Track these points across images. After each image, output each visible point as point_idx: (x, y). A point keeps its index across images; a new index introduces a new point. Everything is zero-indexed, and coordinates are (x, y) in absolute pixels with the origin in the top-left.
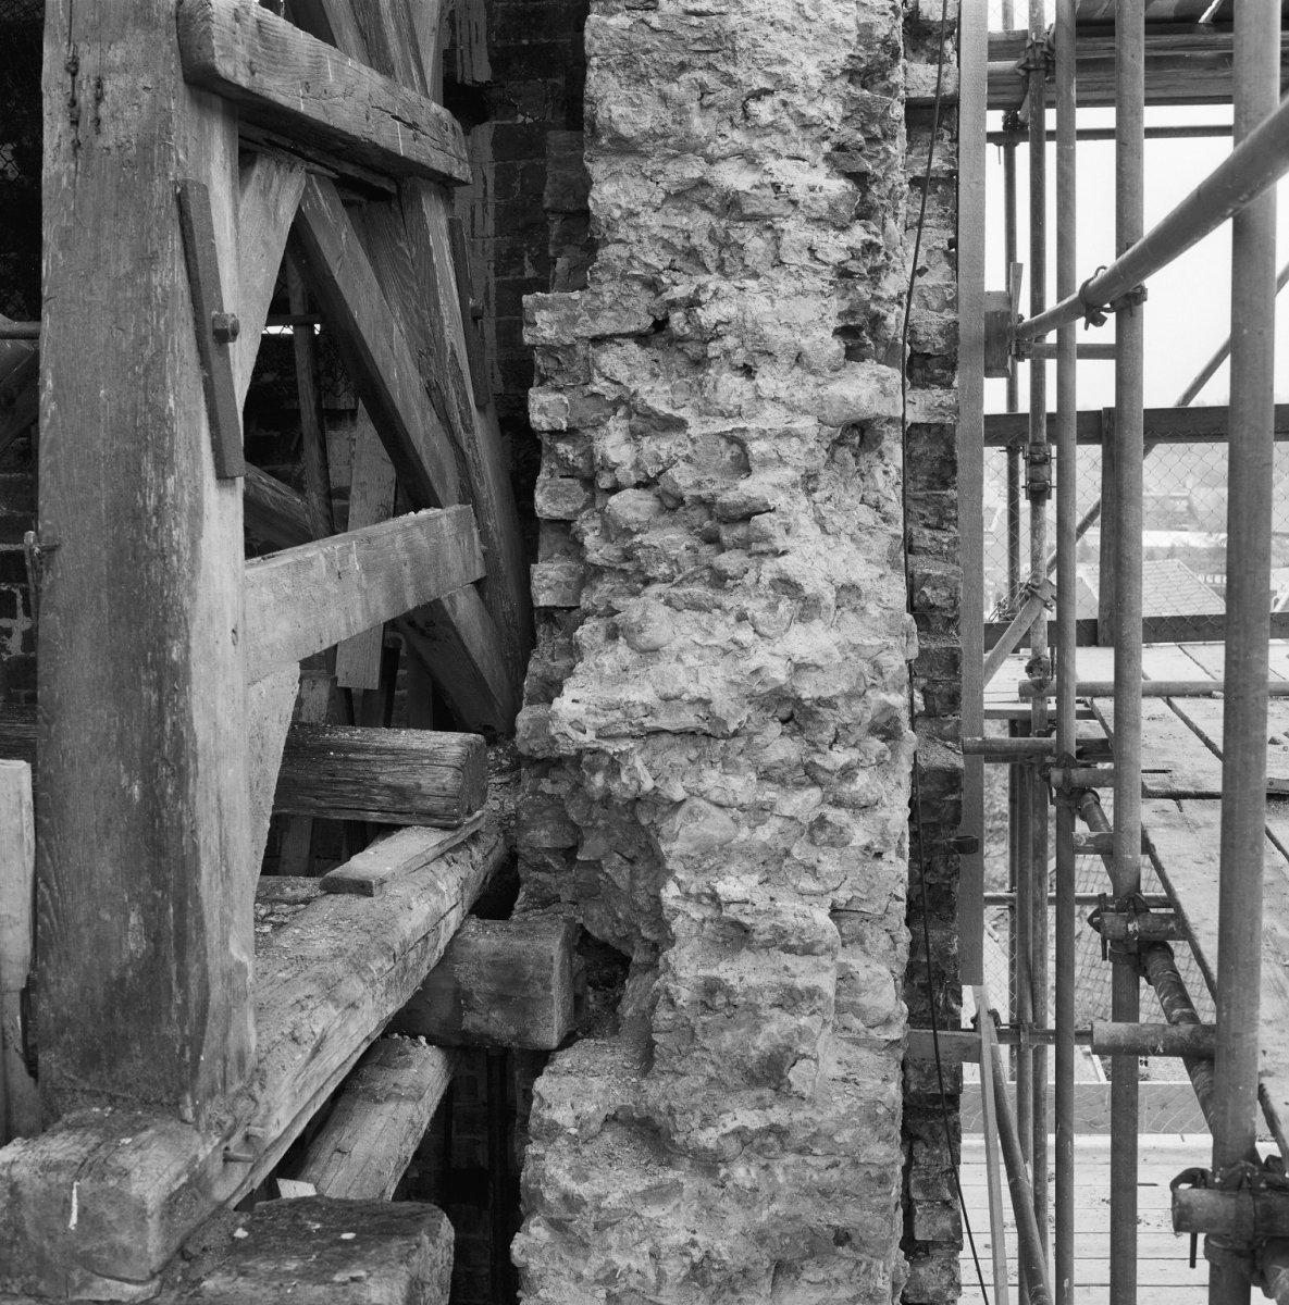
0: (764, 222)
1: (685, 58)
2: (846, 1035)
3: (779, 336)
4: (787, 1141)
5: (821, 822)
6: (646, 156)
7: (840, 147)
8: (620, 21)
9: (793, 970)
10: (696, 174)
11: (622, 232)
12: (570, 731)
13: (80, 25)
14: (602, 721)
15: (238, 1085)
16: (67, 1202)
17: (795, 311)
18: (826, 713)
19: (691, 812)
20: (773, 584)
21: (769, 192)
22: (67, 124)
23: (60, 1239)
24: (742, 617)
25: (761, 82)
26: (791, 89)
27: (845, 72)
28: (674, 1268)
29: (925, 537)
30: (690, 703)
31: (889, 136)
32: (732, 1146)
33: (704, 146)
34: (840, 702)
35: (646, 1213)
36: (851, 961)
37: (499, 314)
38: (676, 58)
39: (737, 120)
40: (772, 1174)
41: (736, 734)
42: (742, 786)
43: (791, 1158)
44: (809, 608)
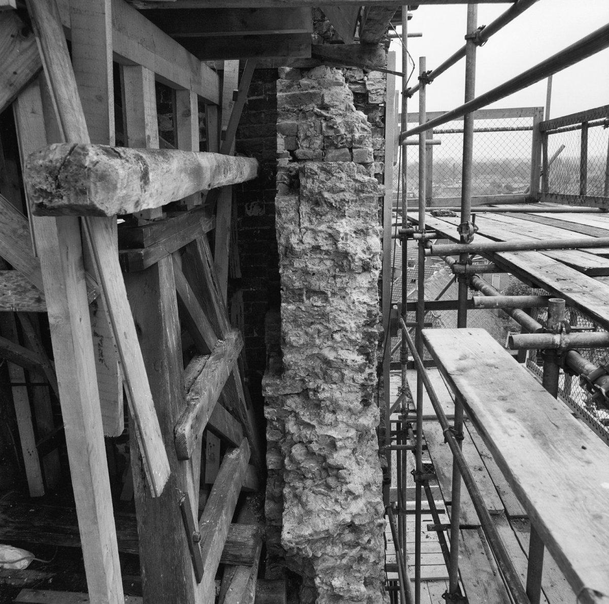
0: (338, 370)
1: (313, 321)
3: (344, 404)
8: (291, 307)
11: (293, 368)
12: (288, 543)
14: (297, 540)
21: (340, 361)
22: (141, 479)
24: (336, 501)
38: (310, 320)
42: (337, 550)
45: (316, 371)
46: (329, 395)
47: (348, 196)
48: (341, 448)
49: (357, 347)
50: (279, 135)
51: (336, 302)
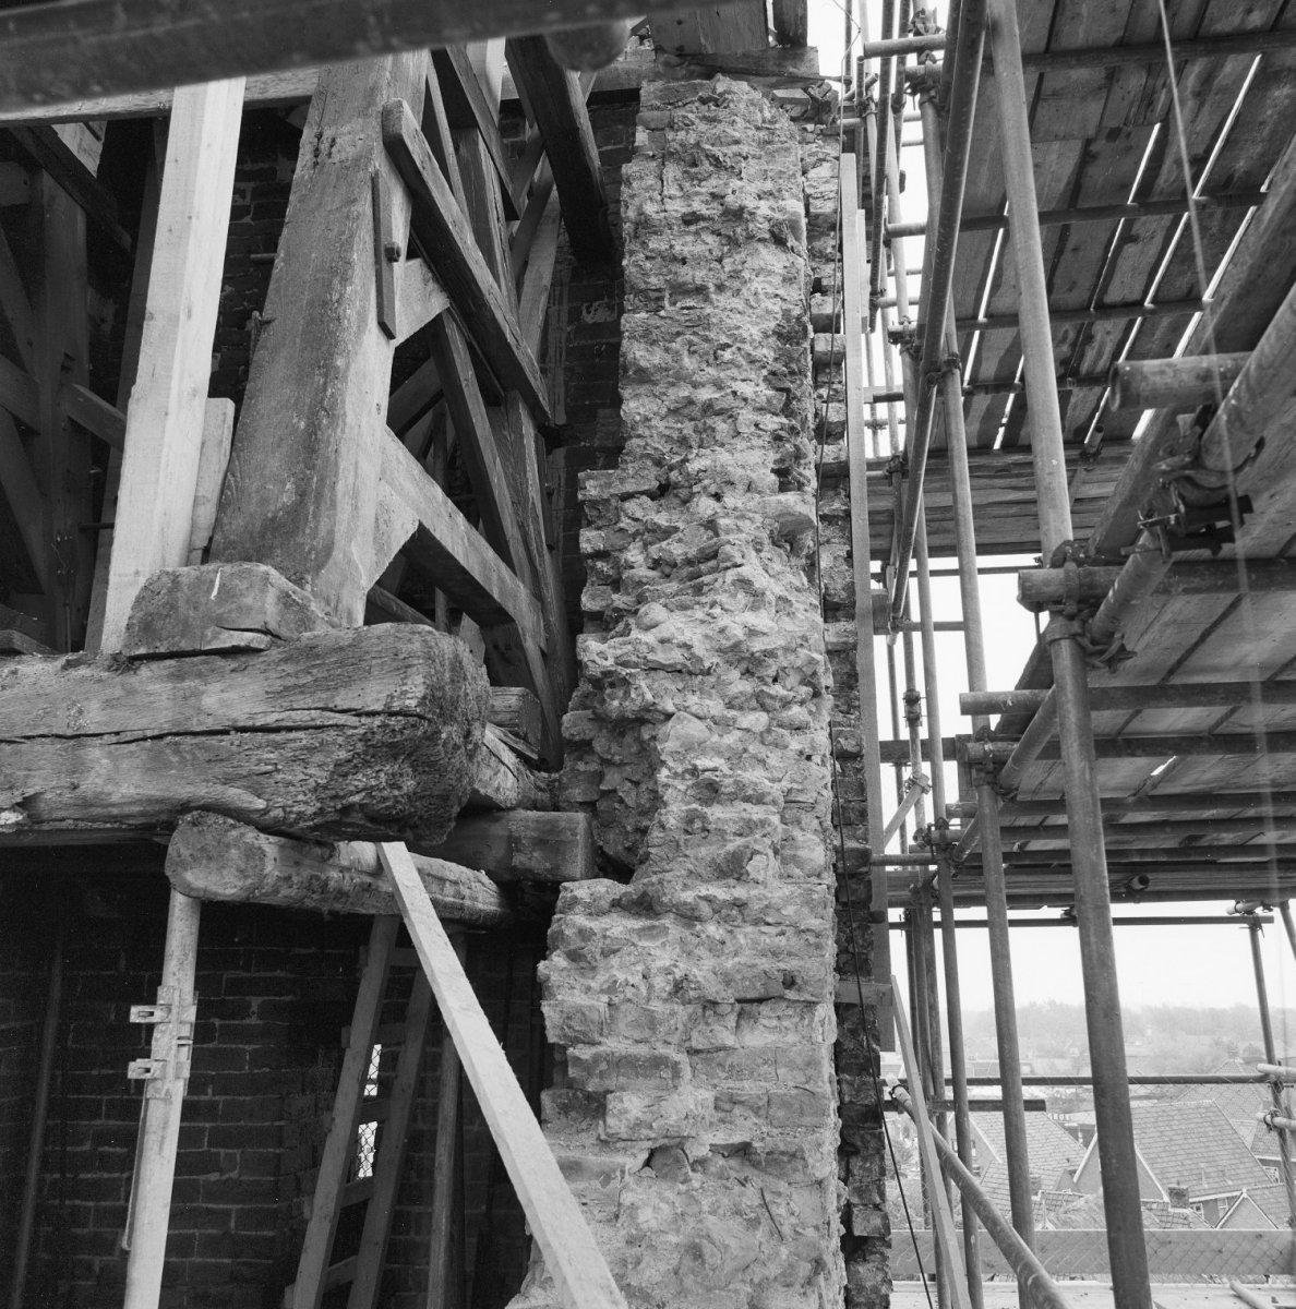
0: (728, 414)
2: (789, 880)
3: (736, 473)
4: (746, 912)
6: (655, 383)
7: (773, 373)
10: (686, 394)
13: (326, 120)
14: (619, 652)
16: (212, 582)
17: (752, 460)
19: (678, 718)
20: (733, 584)
23: (202, 608)
25: (724, 340)
26: (743, 341)
27: (774, 332)
28: (662, 984)
30: (679, 646)
31: (802, 373)
33: (691, 376)
34: (780, 653)
35: (640, 944)
37: (565, 553)
38: (674, 330)
39: (711, 361)
40: (735, 937)
43: (749, 929)
46: (708, 462)
47: (744, 149)
49: (765, 372)
50: (640, 128)
51: (723, 300)
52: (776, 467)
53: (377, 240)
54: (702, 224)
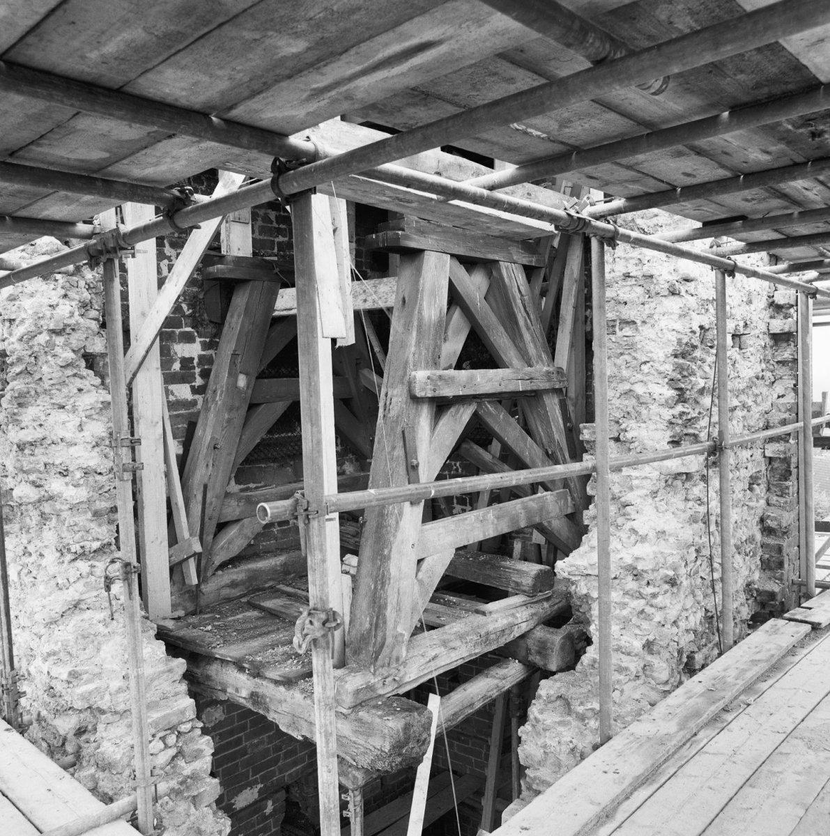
1: (622, 351)
5: (642, 611)
9: (623, 660)
13: (389, 384)
14: (570, 570)
15: (394, 665)
18: (645, 575)
20: (630, 530)
21: (648, 395)
25: (645, 359)
27: (672, 355)
28: (565, 749)
29: (774, 499)
32: (590, 714)
36: (654, 660)
38: (619, 351)
41: (615, 578)
44: (644, 539)
45: (628, 410)
48: (637, 487)
52: (671, 440)
53: (407, 463)
54: (633, 281)
